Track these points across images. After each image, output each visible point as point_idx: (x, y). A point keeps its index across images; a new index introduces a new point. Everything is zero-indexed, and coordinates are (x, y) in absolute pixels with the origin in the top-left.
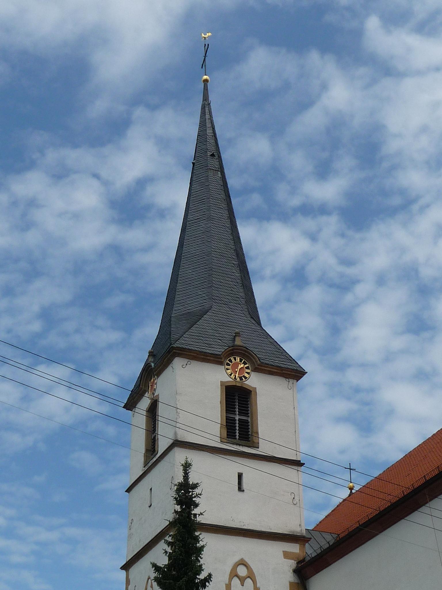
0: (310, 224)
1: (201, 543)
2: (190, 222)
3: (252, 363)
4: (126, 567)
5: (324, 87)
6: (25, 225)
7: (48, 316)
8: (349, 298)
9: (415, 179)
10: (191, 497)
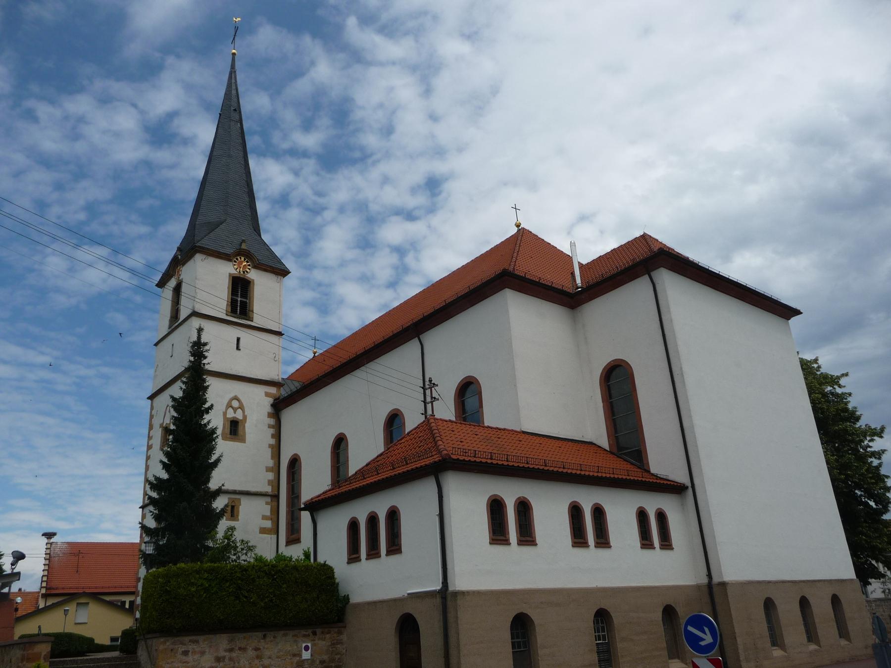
0: (295, 163)
1: (207, 384)
3: (253, 262)
4: (152, 397)
5: (313, 63)
6: (75, 136)
7: (91, 209)
8: (319, 220)
9: (371, 140)
10: (202, 352)
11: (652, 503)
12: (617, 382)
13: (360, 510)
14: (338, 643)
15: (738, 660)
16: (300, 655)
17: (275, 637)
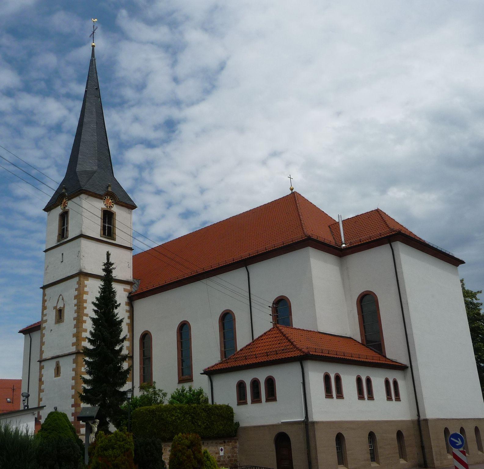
2: (85, 123)
4: (44, 288)
11: (392, 375)
12: (367, 305)
13: (247, 377)
14: (235, 448)
15: (433, 459)
16: (219, 453)
17: (207, 444)
